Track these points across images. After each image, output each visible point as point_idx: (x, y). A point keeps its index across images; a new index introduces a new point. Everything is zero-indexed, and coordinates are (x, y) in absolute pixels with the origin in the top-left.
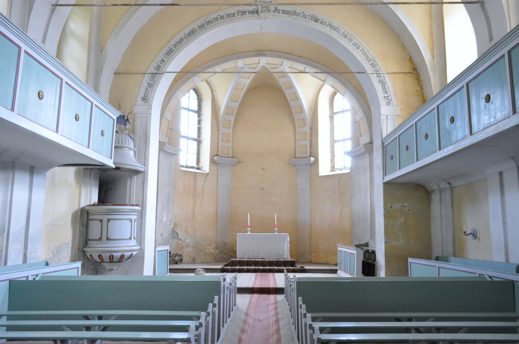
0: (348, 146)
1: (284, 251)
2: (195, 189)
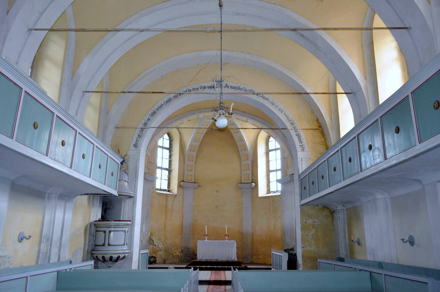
0: (279, 175)
1: (232, 255)
2: (166, 207)
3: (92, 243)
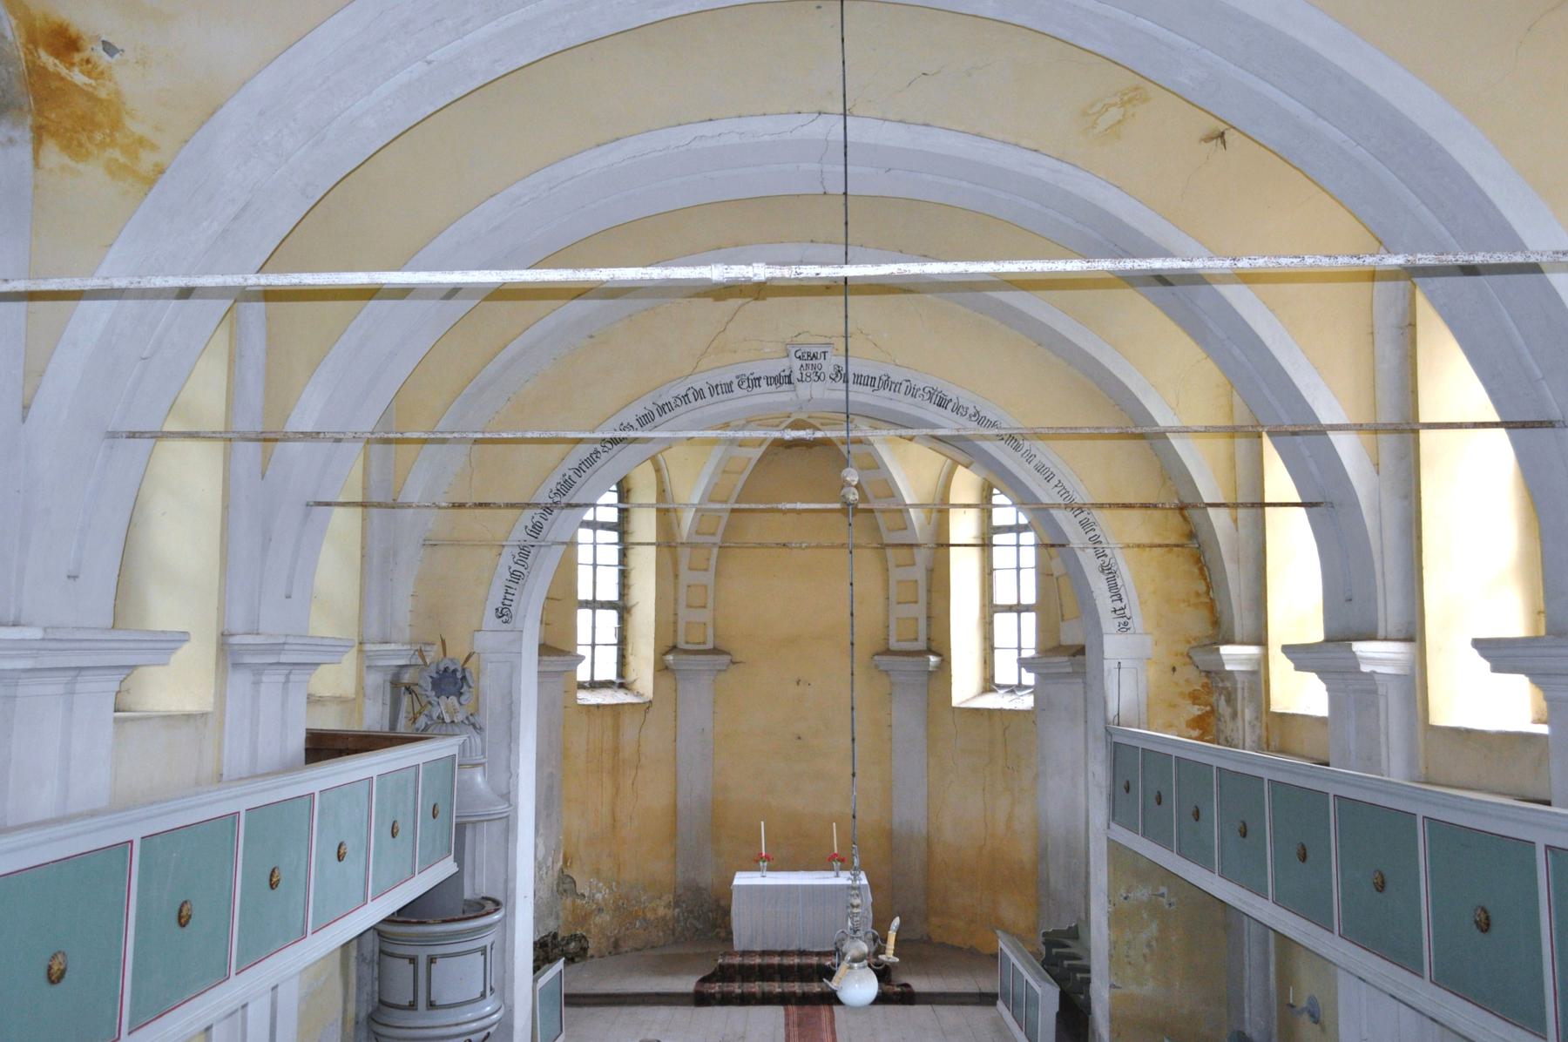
2: (616, 751)
3: (368, 988)
